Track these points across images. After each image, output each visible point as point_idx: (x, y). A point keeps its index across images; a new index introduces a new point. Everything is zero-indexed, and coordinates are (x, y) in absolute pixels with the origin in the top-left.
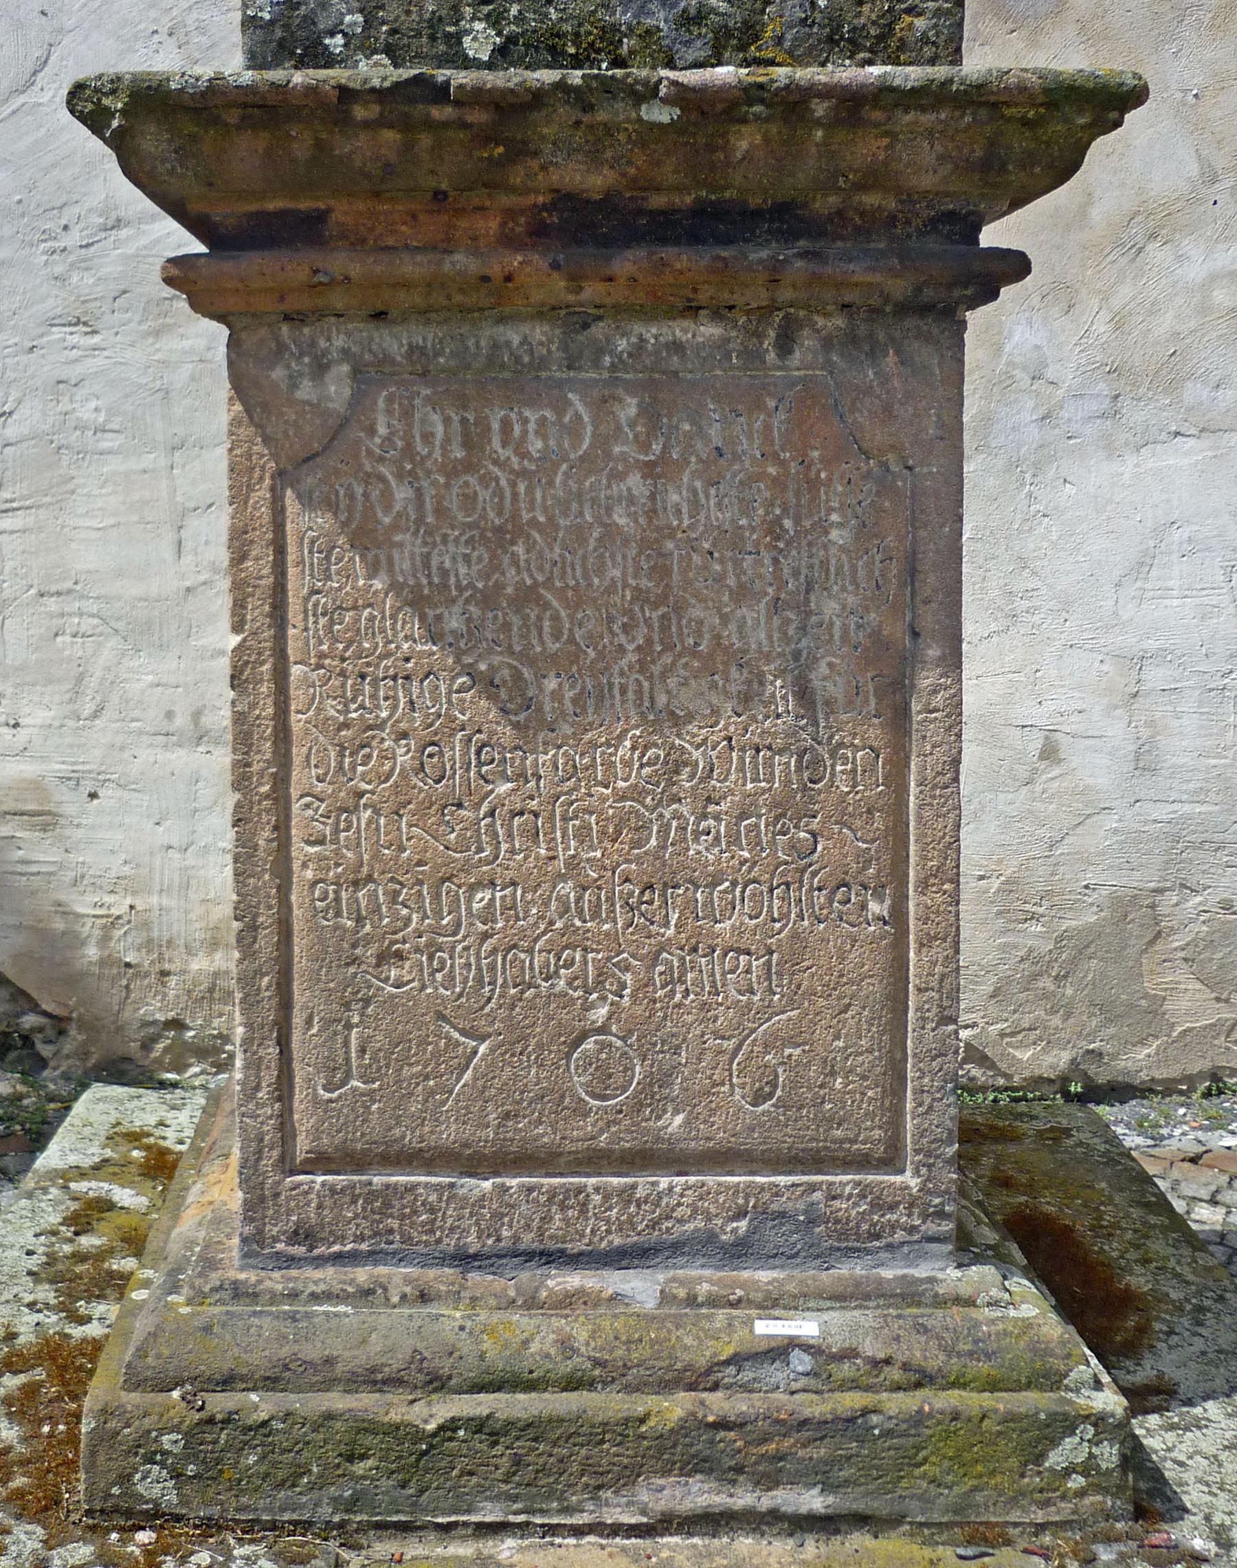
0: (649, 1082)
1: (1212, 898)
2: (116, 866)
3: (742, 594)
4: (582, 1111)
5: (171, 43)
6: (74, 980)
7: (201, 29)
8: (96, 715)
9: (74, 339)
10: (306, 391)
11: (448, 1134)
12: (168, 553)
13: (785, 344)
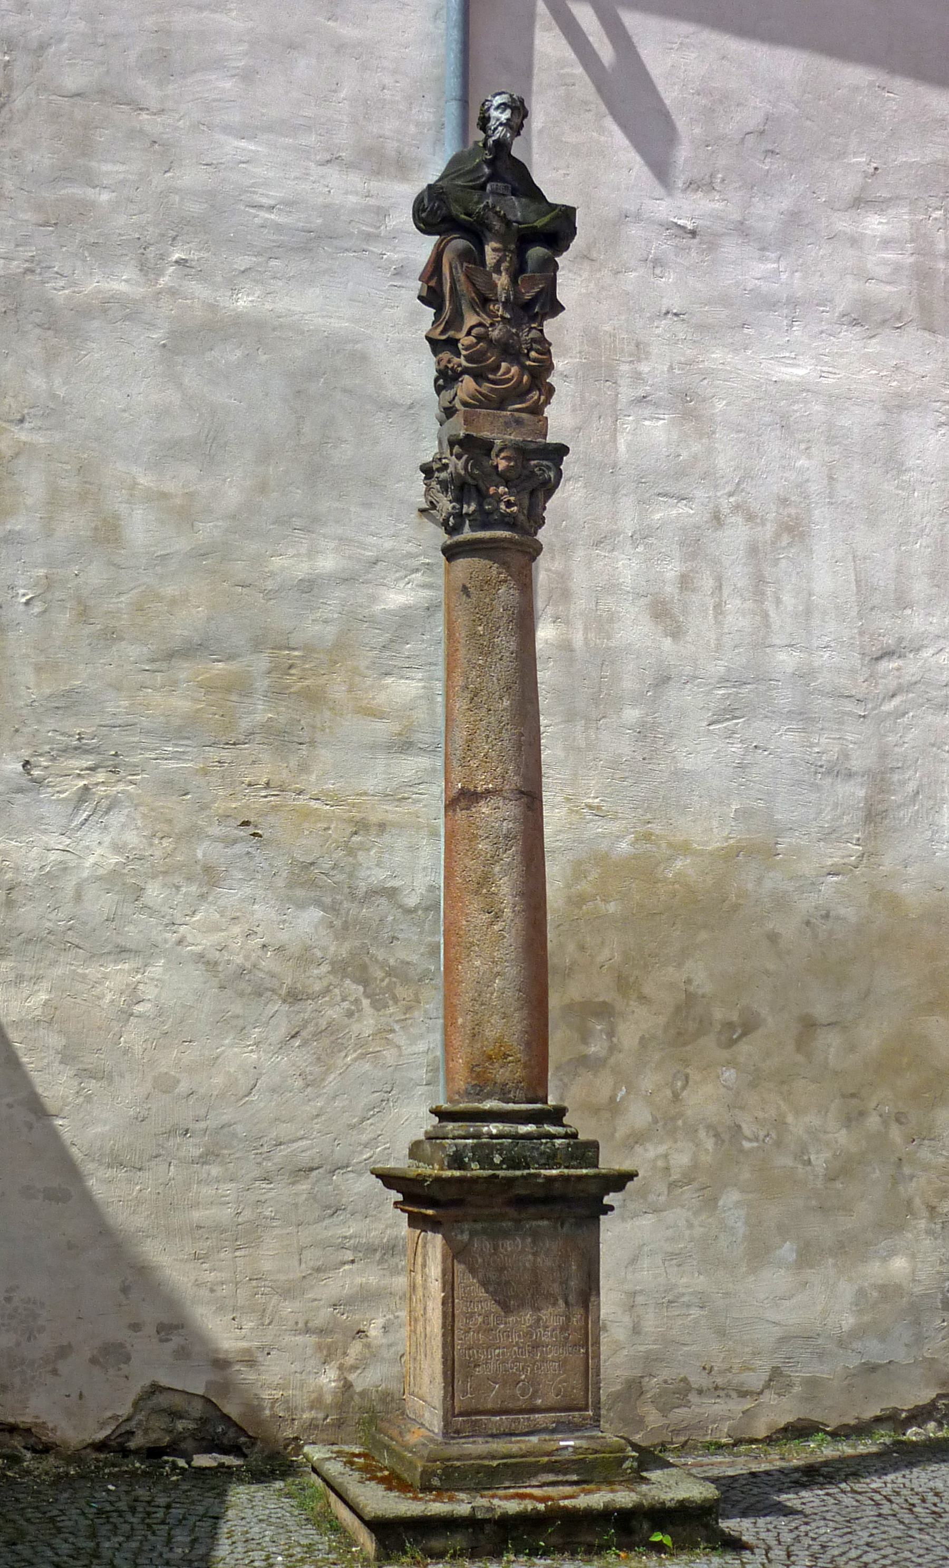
0: (533, 1394)
1: (660, 1379)
2: (276, 1380)
3: (554, 1281)
4: (519, 1399)
5: (300, 1079)
6: (260, 1423)
7: (311, 1074)
8: (269, 1324)
9: (264, 1186)
10: (459, 1237)
11: (489, 1406)
12: (296, 1263)
13: (562, 1225)
